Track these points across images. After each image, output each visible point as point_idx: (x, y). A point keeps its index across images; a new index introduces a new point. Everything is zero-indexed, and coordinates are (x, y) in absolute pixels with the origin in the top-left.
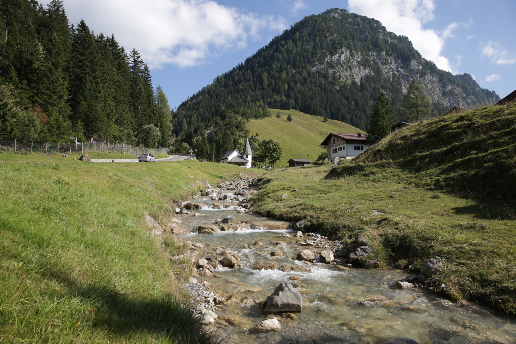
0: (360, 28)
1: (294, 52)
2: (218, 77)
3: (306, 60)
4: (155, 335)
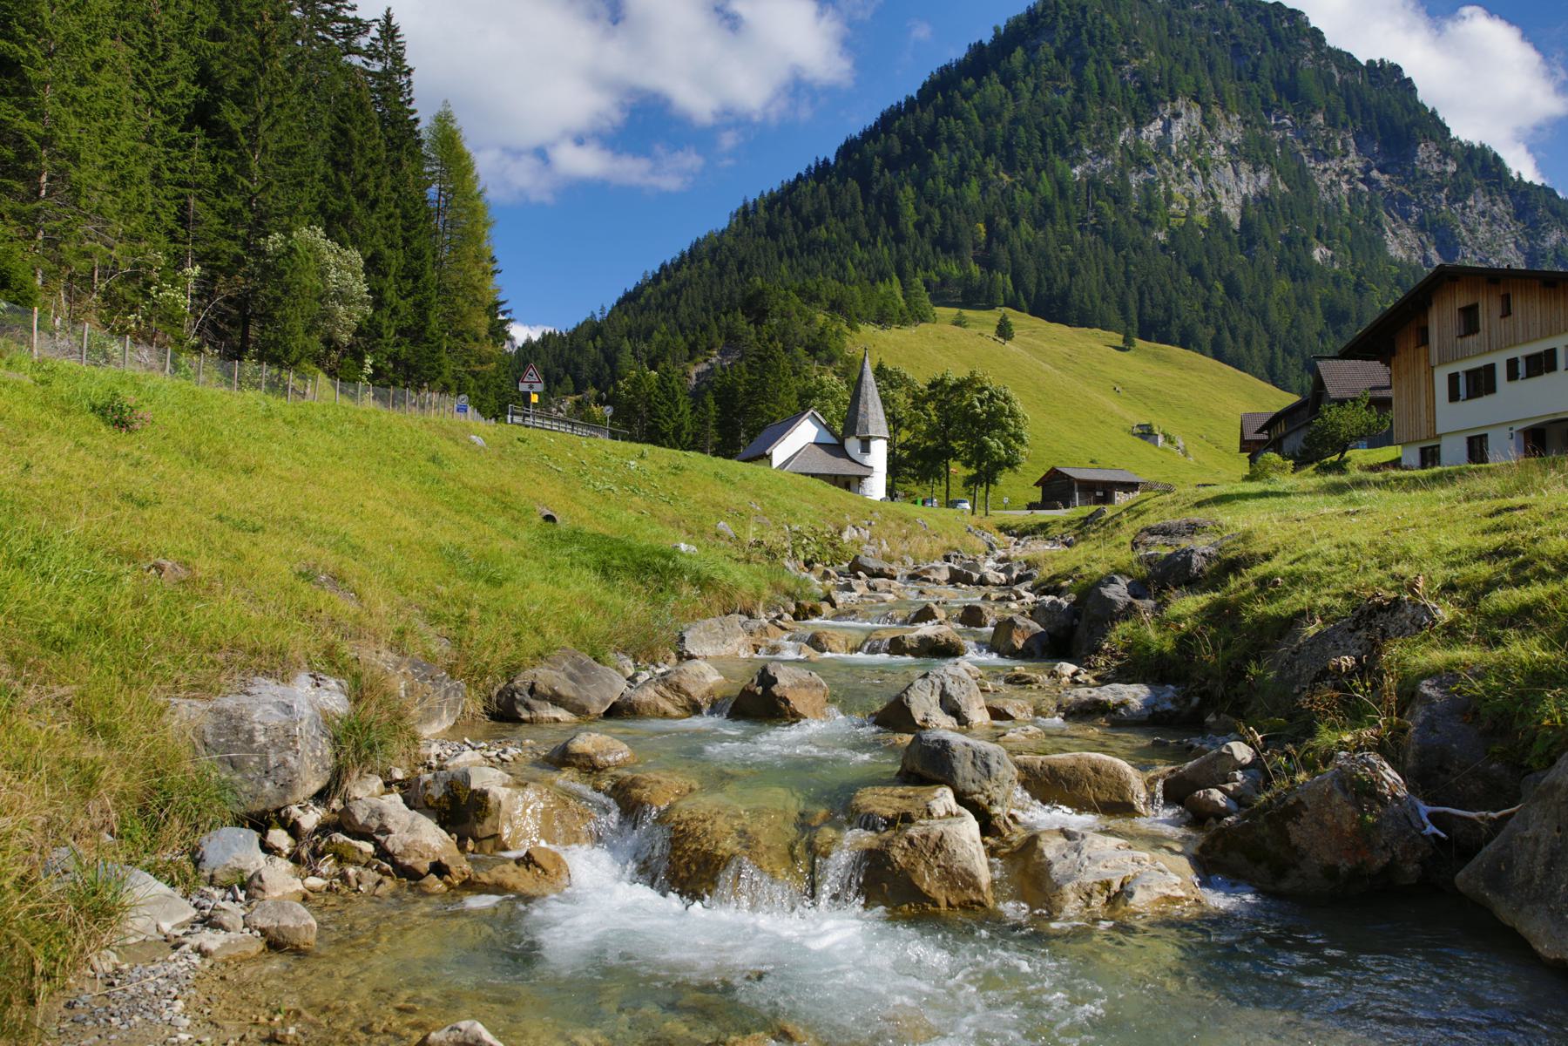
0: (1233, 36)
2: (745, 206)
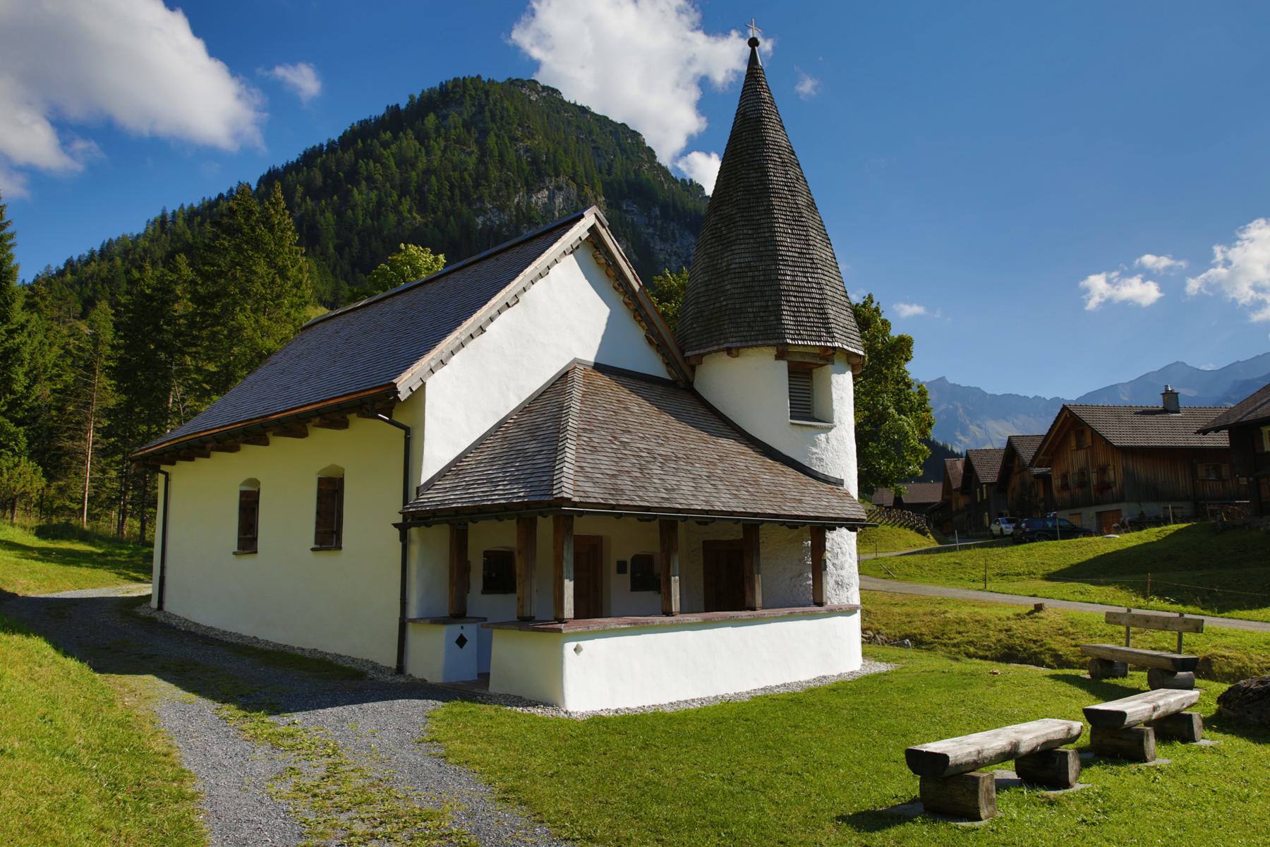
0: (593, 141)
1: (421, 166)
2: (164, 216)
3: (457, 191)
4: (417, 96)
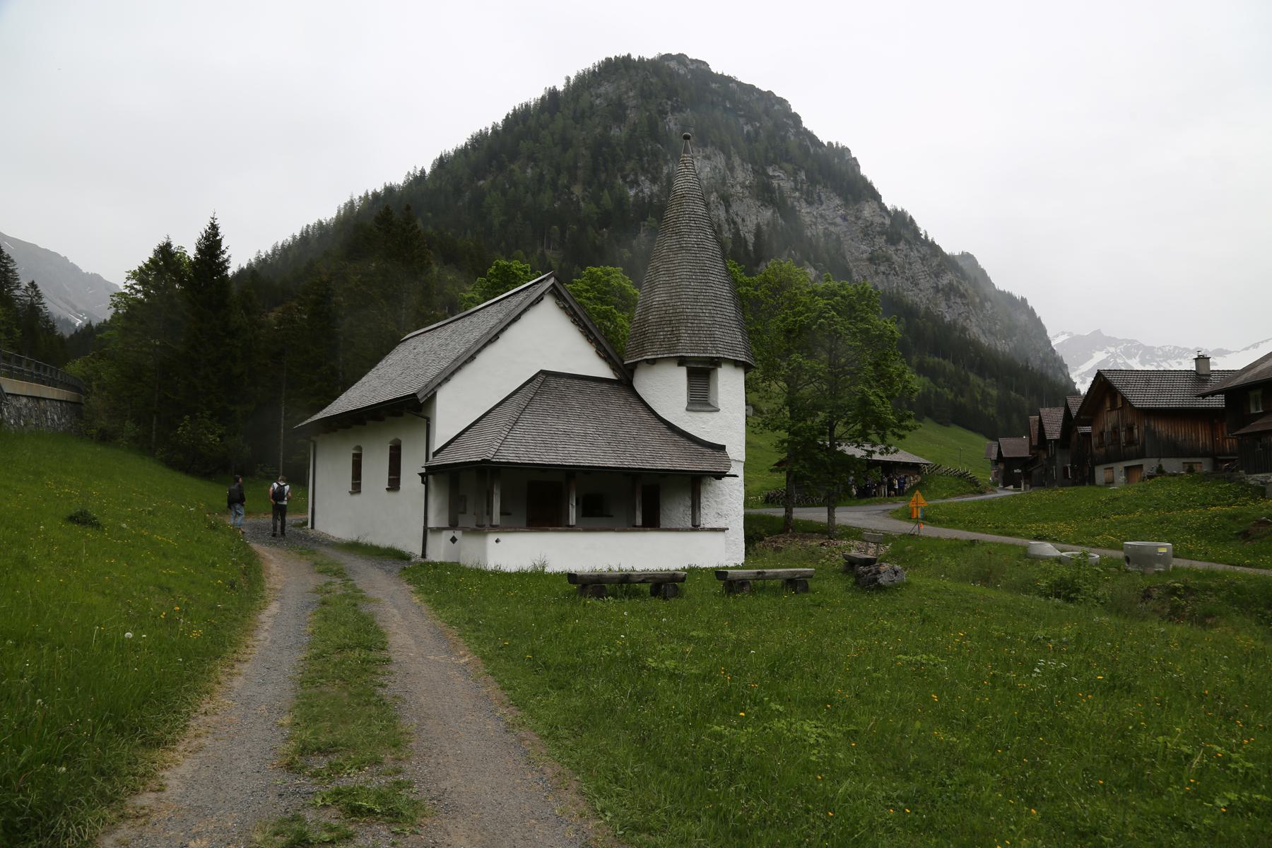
4: (572, 78)
